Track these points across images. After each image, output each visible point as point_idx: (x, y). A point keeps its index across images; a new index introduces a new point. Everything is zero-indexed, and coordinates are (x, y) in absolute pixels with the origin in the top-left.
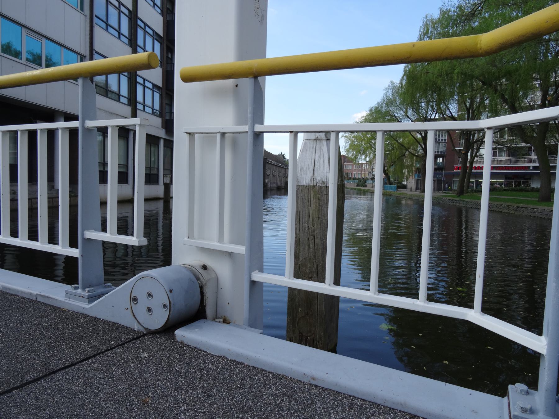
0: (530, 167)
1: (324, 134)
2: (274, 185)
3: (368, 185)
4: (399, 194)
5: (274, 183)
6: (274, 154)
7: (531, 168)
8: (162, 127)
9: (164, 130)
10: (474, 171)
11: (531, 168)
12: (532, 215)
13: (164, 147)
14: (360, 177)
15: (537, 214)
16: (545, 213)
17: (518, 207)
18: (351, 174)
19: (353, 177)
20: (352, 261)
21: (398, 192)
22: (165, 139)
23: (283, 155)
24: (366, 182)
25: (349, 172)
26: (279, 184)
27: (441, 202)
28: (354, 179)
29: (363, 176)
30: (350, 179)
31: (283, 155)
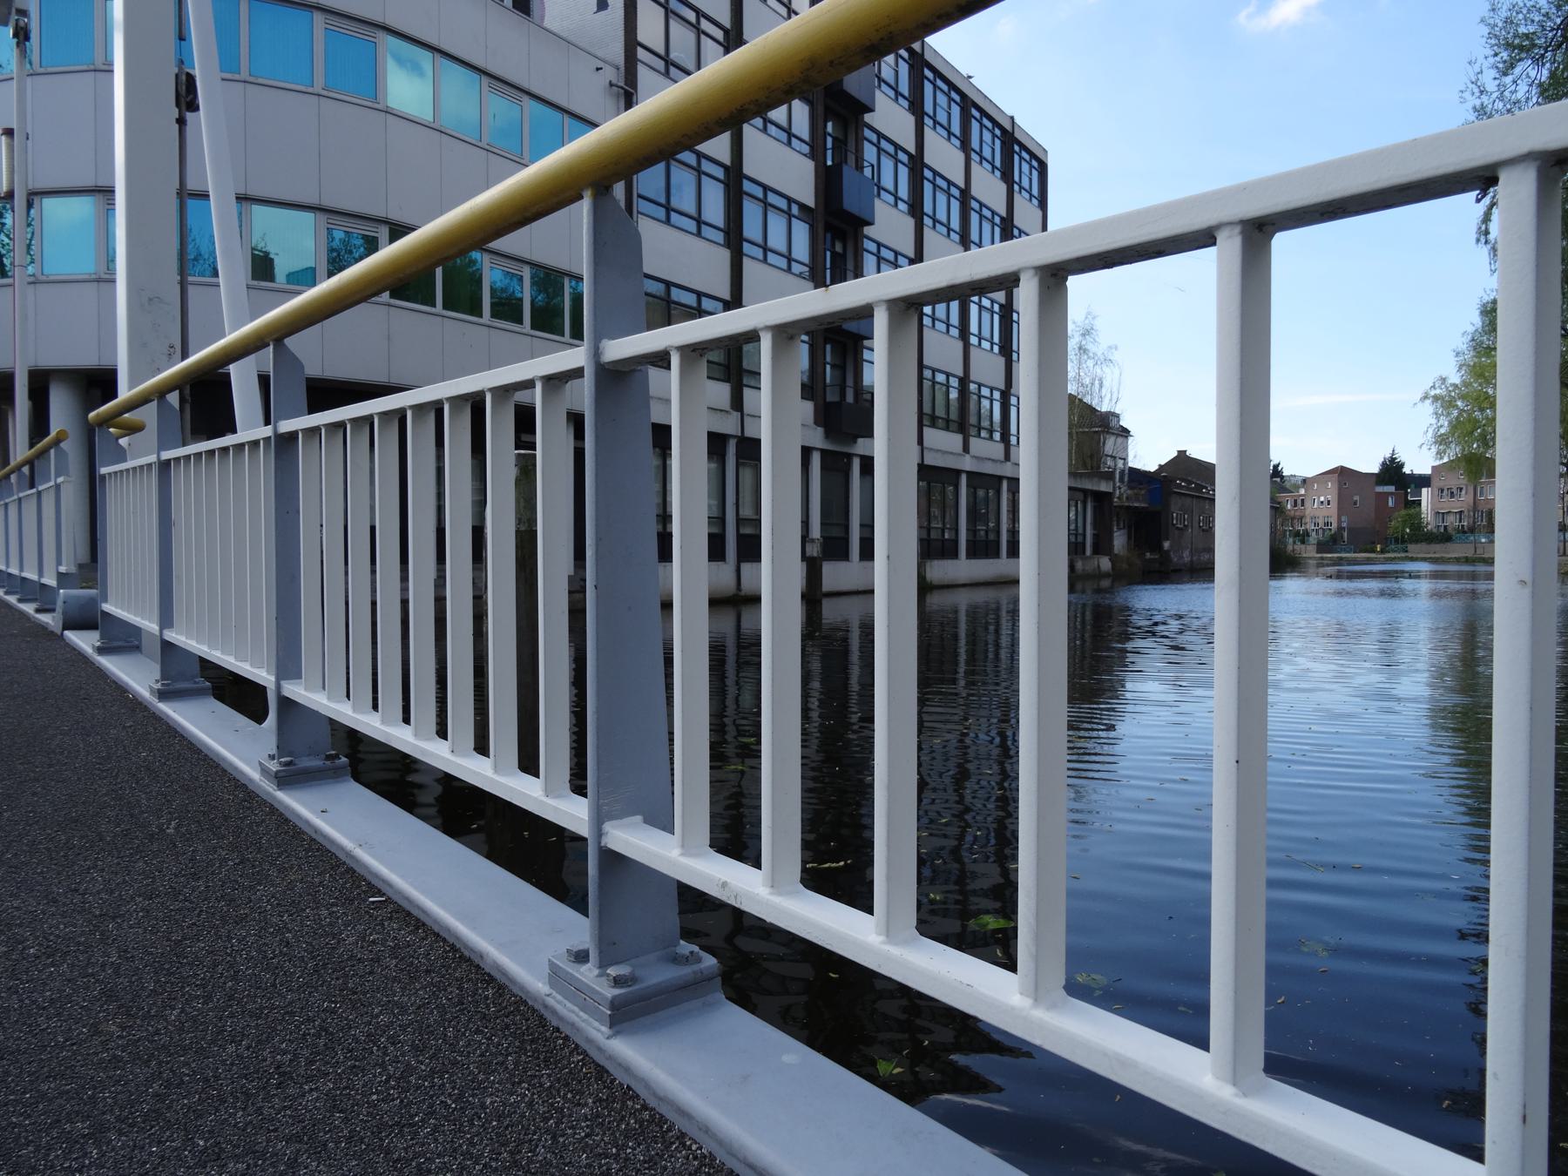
8: (816, 423)
9: (820, 430)
22: (823, 451)
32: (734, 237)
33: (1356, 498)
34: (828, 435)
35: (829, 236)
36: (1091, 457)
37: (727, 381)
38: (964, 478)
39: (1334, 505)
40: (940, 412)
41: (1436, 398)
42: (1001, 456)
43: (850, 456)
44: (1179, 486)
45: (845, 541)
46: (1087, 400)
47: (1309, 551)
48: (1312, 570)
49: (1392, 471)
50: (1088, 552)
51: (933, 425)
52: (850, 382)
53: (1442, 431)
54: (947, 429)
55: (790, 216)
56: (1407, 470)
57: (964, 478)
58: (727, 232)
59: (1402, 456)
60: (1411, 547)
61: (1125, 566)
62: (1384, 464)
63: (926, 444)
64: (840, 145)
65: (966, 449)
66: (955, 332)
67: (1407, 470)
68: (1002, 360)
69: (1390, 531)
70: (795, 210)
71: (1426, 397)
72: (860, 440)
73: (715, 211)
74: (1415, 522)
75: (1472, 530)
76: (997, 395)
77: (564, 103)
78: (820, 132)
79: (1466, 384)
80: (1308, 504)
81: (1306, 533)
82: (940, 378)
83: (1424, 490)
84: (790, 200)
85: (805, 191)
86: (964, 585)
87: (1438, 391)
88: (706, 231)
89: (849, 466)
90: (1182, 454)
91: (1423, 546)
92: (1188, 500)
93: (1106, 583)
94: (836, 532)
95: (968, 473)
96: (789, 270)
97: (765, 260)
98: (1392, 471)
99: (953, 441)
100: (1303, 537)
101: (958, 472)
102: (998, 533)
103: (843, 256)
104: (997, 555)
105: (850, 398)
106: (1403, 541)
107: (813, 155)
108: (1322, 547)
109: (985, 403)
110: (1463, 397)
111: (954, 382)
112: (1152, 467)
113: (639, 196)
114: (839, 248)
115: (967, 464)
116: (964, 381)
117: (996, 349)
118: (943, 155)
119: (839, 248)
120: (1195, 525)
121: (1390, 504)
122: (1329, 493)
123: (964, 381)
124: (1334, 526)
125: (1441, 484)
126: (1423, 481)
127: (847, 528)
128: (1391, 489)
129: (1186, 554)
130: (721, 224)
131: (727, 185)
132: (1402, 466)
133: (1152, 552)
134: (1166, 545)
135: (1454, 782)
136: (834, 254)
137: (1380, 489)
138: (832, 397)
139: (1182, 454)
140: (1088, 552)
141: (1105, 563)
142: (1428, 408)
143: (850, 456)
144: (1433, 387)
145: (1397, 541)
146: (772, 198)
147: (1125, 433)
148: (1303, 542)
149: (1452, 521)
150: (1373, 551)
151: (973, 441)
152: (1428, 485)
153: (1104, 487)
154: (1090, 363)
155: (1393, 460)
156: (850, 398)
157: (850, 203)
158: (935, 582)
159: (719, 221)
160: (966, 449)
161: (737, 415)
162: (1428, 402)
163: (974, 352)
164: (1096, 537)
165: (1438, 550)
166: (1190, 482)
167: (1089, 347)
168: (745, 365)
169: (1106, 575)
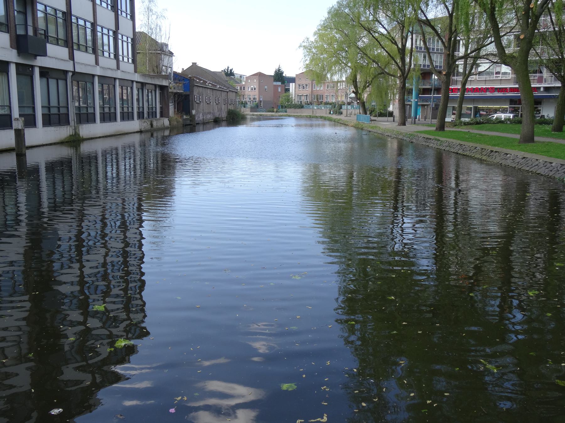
0: (539, 88)
1: (8, 104)
2: (209, 116)
3: (344, 112)
4: (372, 127)
5: (210, 113)
6: (213, 70)
7: (542, 89)
8: (11, 47)
9: (15, 52)
10: (467, 95)
11: (542, 89)
12: (504, 162)
13: (17, 74)
14: (334, 101)
15: (509, 162)
16: (517, 160)
17: (492, 151)
18: (322, 96)
19: (325, 100)
20: (316, 220)
21: (373, 124)
22: (17, 64)
23: (231, 70)
24: (341, 108)
25: (319, 93)
26: (217, 115)
27: (414, 141)
28: (326, 104)
29: (339, 100)
30: (321, 103)
31: (231, 70)
33: (266, 87)
36: (157, 67)
38: (96, 79)
39: (257, 90)
40: (82, 42)
41: (305, 47)
42: (115, 67)
43: (33, 67)
44: (198, 82)
46: (153, 37)
47: (246, 111)
48: (248, 120)
49: (279, 76)
51: (79, 49)
52: (30, 22)
53: (308, 62)
54: (86, 51)
56: (284, 75)
57: (96, 79)
59: (283, 69)
60: (288, 110)
61: (175, 123)
62: (276, 71)
65: (97, 63)
66: (129, 17)
67: (284, 75)
69: (280, 103)
71: (300, 46)
74: (288, 100)
75: (311, 104)
76: (111, 33)
79: (316, 42)
80: (246, 89)
81: (246, 103)
82: (81, 22)
83: (291, 84)
86: (100, 137)
87: (305, 44)
89: (33, 72)
90: (194, 64)
91: (292, 110)
92: (201, 89)
93: (167, 133)
94: (29, 111)
95: (99, 76)
98: (279, 76)
99: (89, 58)
100: (244, 104)
101: (93, 76)
105: (31, 32)
106: (286, 107)
108: (253, 109)
109: (105, 38)
110: (315, 48)
111: (88, 25)
112: (179, 71)
115: (98, 71)
116: (94, 25)
117: (109, 7)
120: (204, 101)
121: (279, 90)
122: (255, 84)
123: (94, 25)
124: (257, 100)
125: (299, 83)
126: (292, 80)
127: (34, 109)
128: (279, 83)
129: (201, 115)
132: (283, 73)
133: (186, 114)
134: (194, 112)
135: (318, 222)
137: (275, 83)
138: (20, 32)
139: (194, 64)
141: (166, 122)
142: (302, 51)
144: (304, 42)
145: (282, 107)
147: (171, 54)
148: (245, 107)
149: (303, 99)
150: (273, 112)
151: (101, 59)
152: (294, 82)
153: (165, 83)
154: (154, 17)
155: (279, 70)
158: (85, 137)
160: (97, 63)
162: (302, 48)
163: (98, 8)
164: (161, 108)
165: (299, 112)
166: (201, 80)
167: (153, 8)
169: (167, 128)
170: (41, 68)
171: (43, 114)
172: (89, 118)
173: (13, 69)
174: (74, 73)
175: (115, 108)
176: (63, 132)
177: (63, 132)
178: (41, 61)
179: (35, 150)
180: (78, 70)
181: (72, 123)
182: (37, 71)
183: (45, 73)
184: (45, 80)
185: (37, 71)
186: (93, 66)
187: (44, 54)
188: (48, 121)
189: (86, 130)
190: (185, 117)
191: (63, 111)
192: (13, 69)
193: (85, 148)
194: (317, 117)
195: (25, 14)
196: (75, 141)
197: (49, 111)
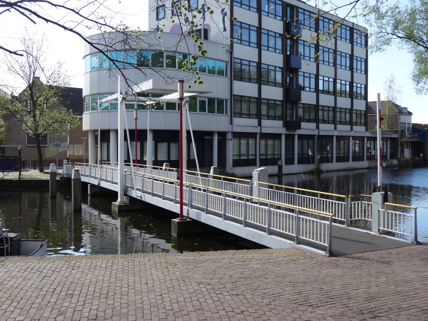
8: (283, 127)
9: (285, 129)
22: (286, 134)
32: (259, 45)
34: (287, 130)
35: (288, 72)
37: (257, 83)
43: (294, 135)
45: (293, 159)
50: (388, 158)
55: (275, 37)
58: (257, 9)
63: (320, 128)
64: (292, 17)
65: (335, 129)
68: (350, 72)
70: (277, 35)
72: (297, 130)
73: (254, 38)
77: (216, 58)
78: (285, 44)
84: (275, 33)
85: (280, 30)
86: (336, 171)
88: (251, 9)
90: (40, 77)
95: (352, 136)
96: (275, 52)
97: (268, 16)
101: (333, 136)
102: (349, 154)
103: (293, 78)
104: (348, 161)
107: (282, 20)
113: (234, 58)
114: (291, 76)
118: (327, 42)
119: (291, 76)
127: (281, 154)
130: (256, 7)
131: (257, 102)
136: (290, 78)
138: (288, 119)
140: (388, 158)
141: (395, 162)
143: (294, 135)
146: (270, 33)
156: (294, 119)
157: (293, 65)
159: (255, 6)
160: (335, 129)
161: (259, 127)
168: (262, 9)
169: (396, 166)
170: (298, 135)
171: (336, 157)
172: (329, 160)
173: (283, 137)
174: (319, 136)
175: (332, 154)
176: (310, 167)
177: (310, 167)
178: (298, 132)
179: (292, 176)
180: (321, 133)
181: (316, 162)
182: (296, 137)
183: (301, 137)
184: (301, 141)
185: (296, 137)
186: (349, 131)
187: (300, 128)
188: (301, 162)
189: (325, 167)
190: (416, 158)
191: (361, 154)
192: (283, 137)
193: (323, 176)
194: (161, 181)
195: (293, 110)
196: (319, 172)
197: (302, 156)
